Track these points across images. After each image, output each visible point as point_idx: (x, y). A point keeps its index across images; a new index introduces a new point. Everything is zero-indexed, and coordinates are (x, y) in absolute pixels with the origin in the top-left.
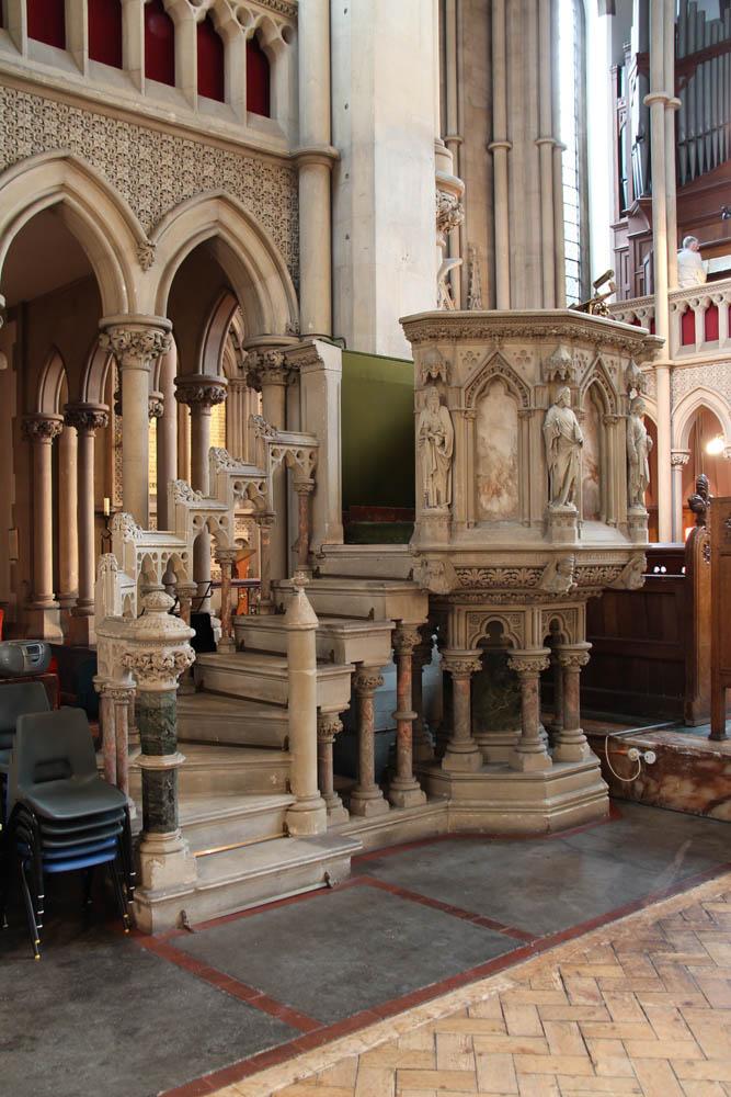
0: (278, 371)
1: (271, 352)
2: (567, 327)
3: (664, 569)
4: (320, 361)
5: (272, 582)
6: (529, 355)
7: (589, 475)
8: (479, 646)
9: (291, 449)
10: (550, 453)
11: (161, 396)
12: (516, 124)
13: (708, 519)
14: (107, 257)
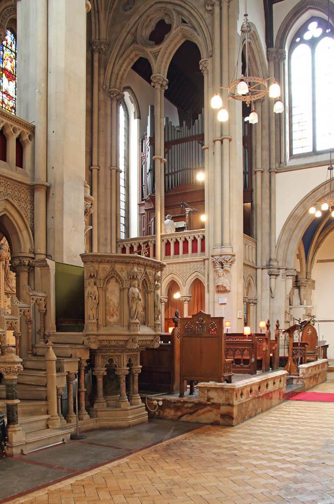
1: (24, 259)
2: (136, 260)
3: (162, 342)
4: (48, 266)
6: (124, 269)
7: (142, 310)
8: (105, 367)
9: (38, 297)
10: (130, 303)
12: (102, 159)
13: (179, 325)
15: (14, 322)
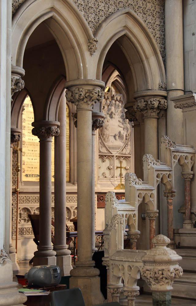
0: (155, 110)
5: (174, 230)
9: (182, 154)
11: (59, 124)
14: (73, 47)
15: (149, 193)
